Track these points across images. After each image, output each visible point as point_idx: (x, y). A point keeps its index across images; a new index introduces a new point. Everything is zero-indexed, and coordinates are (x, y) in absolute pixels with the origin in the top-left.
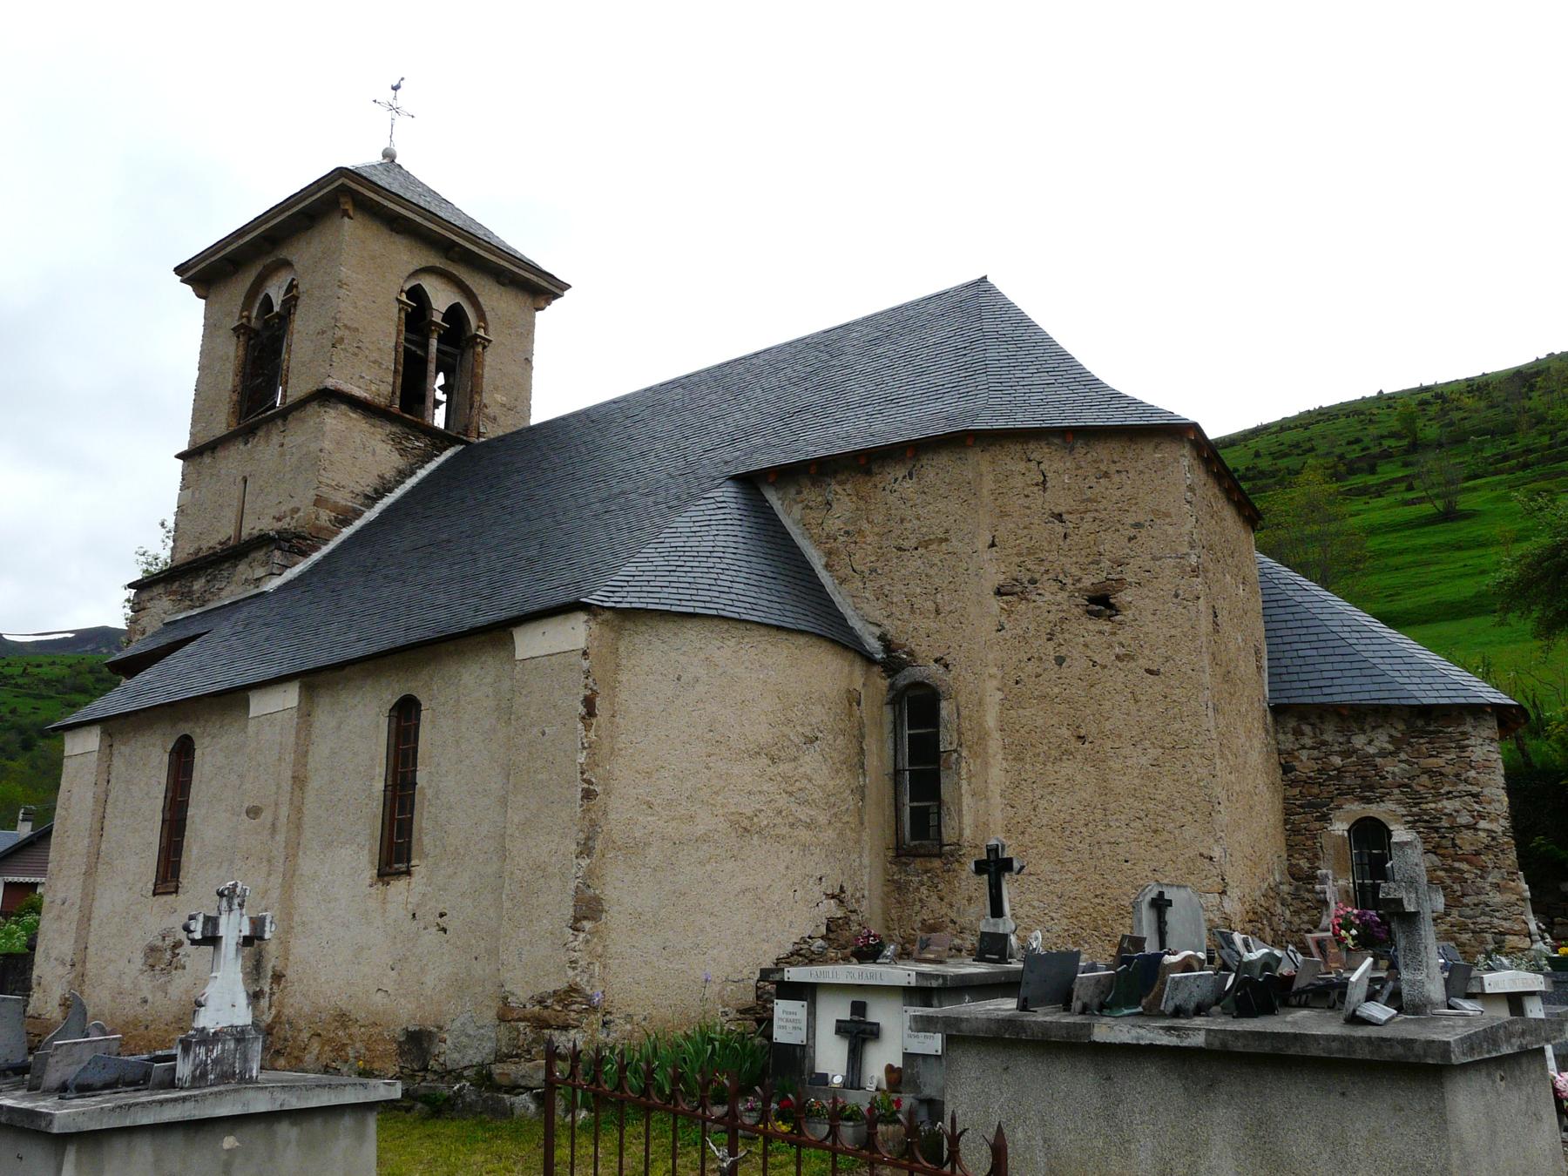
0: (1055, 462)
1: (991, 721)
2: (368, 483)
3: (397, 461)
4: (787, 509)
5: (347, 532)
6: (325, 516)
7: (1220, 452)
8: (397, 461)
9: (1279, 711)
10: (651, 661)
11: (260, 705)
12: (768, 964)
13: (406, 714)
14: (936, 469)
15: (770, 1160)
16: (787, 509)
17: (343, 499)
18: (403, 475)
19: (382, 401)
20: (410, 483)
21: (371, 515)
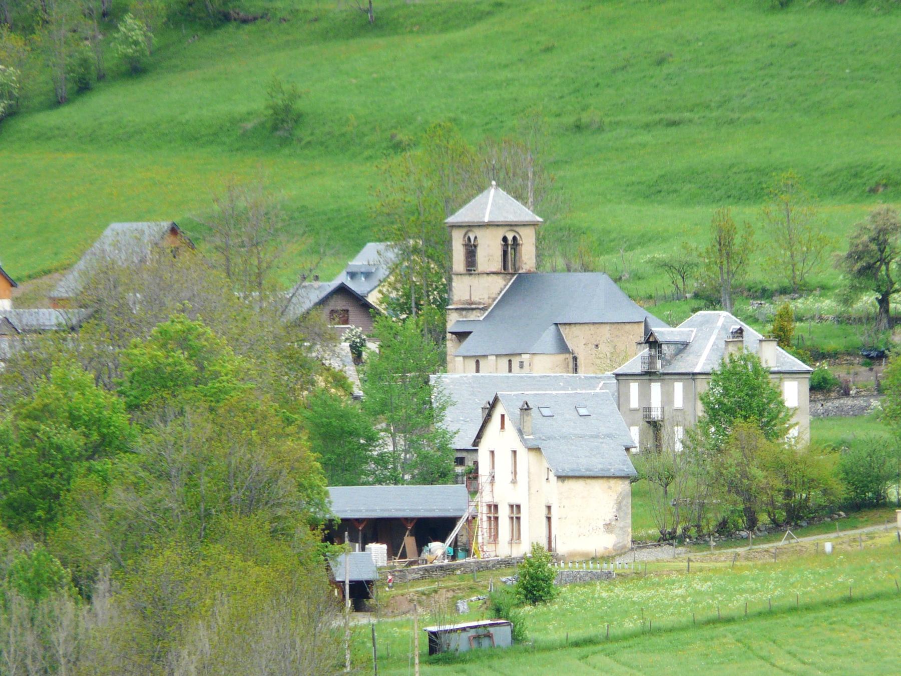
0: (592, 327)
1: (716, 332)
2: (498, 290)
3: (504, 283)
4: (561, 329)
5: (495, 303)
6: (490, 301)
7: (453, 276)
8: (504, 283)
9: (569, 270)
10: (537, 359)
11: (489, 357)
12: (467, 277)
13: (510, 361)
14: (577, 326)
15: (300, 291)
16: (561, 329)
17: (494, 296)
18: (505, 286)
19: (499, 271)
20: (508, 287)
21: (499, 298)
